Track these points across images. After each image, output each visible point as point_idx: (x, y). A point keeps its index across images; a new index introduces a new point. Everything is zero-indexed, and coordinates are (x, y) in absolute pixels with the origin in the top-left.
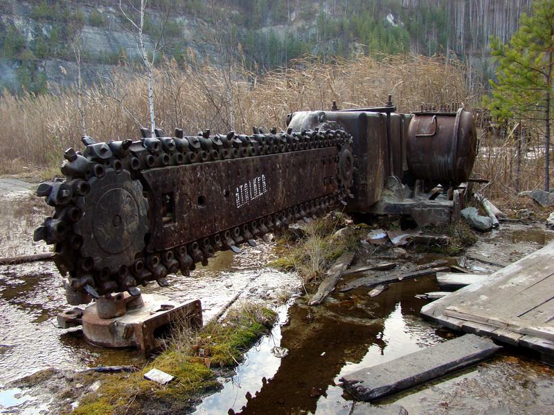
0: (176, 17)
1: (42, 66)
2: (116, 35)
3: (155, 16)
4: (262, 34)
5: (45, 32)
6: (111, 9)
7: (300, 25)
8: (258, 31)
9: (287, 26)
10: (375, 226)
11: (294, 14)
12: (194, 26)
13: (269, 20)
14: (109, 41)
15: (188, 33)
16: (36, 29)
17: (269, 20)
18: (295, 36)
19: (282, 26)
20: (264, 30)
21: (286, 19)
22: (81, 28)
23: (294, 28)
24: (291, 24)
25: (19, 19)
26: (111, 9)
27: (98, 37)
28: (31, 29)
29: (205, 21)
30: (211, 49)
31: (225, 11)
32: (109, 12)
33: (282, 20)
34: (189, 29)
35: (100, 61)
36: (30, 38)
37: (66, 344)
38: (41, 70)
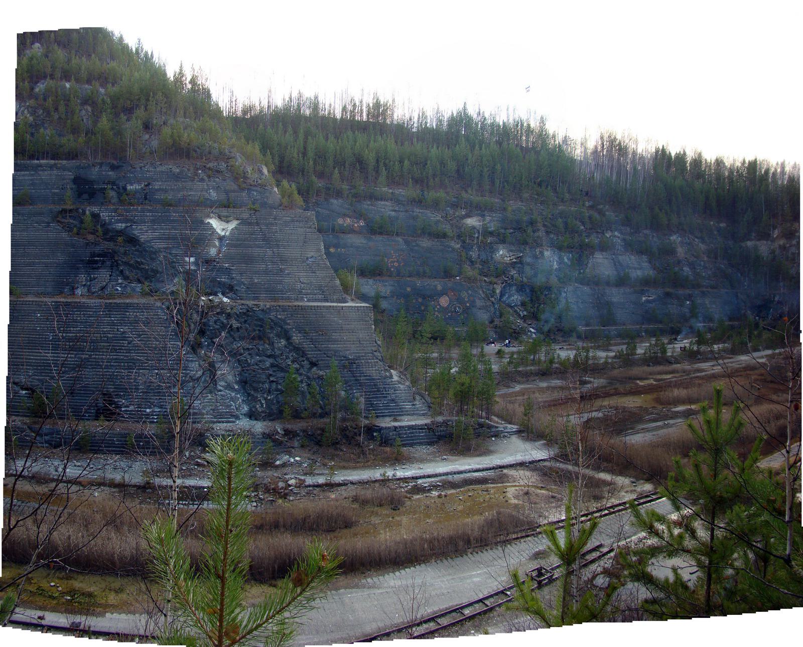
0: (671, 235)
1: (565, 292)
2: (620, 258)
3: (653, 236)
4: (747, 246)
5: (566, 260)
6: (616, 233)
7: (781, 242)
8: (743, 244)
9: (769, 243)
10: (473, 632)
11: (776, 232)
12: (686, 243)
13: (754, 234)
14: (615, 265)
15: (681, 251)
16: (559, 258)
17: (754, 234)
18: (777, 253)
19: (765, 242)
20: (749, 243)
21: (769, 235)
22: (593, 254)
23: (776, 245)
24: (773, 240)
25: (547, 250)
26: (616, 233)
27: (606, 261)
28: (556, 258)
29: (697, 237)
30: (700, 265)
31: (714, 225)
32: (615, 236)
33: (765, 236)
34: (681, 247)
35: (608, 284)
36: (555, 266)
37: (657, 151)
38: (564, 295)
